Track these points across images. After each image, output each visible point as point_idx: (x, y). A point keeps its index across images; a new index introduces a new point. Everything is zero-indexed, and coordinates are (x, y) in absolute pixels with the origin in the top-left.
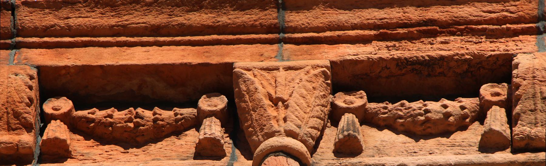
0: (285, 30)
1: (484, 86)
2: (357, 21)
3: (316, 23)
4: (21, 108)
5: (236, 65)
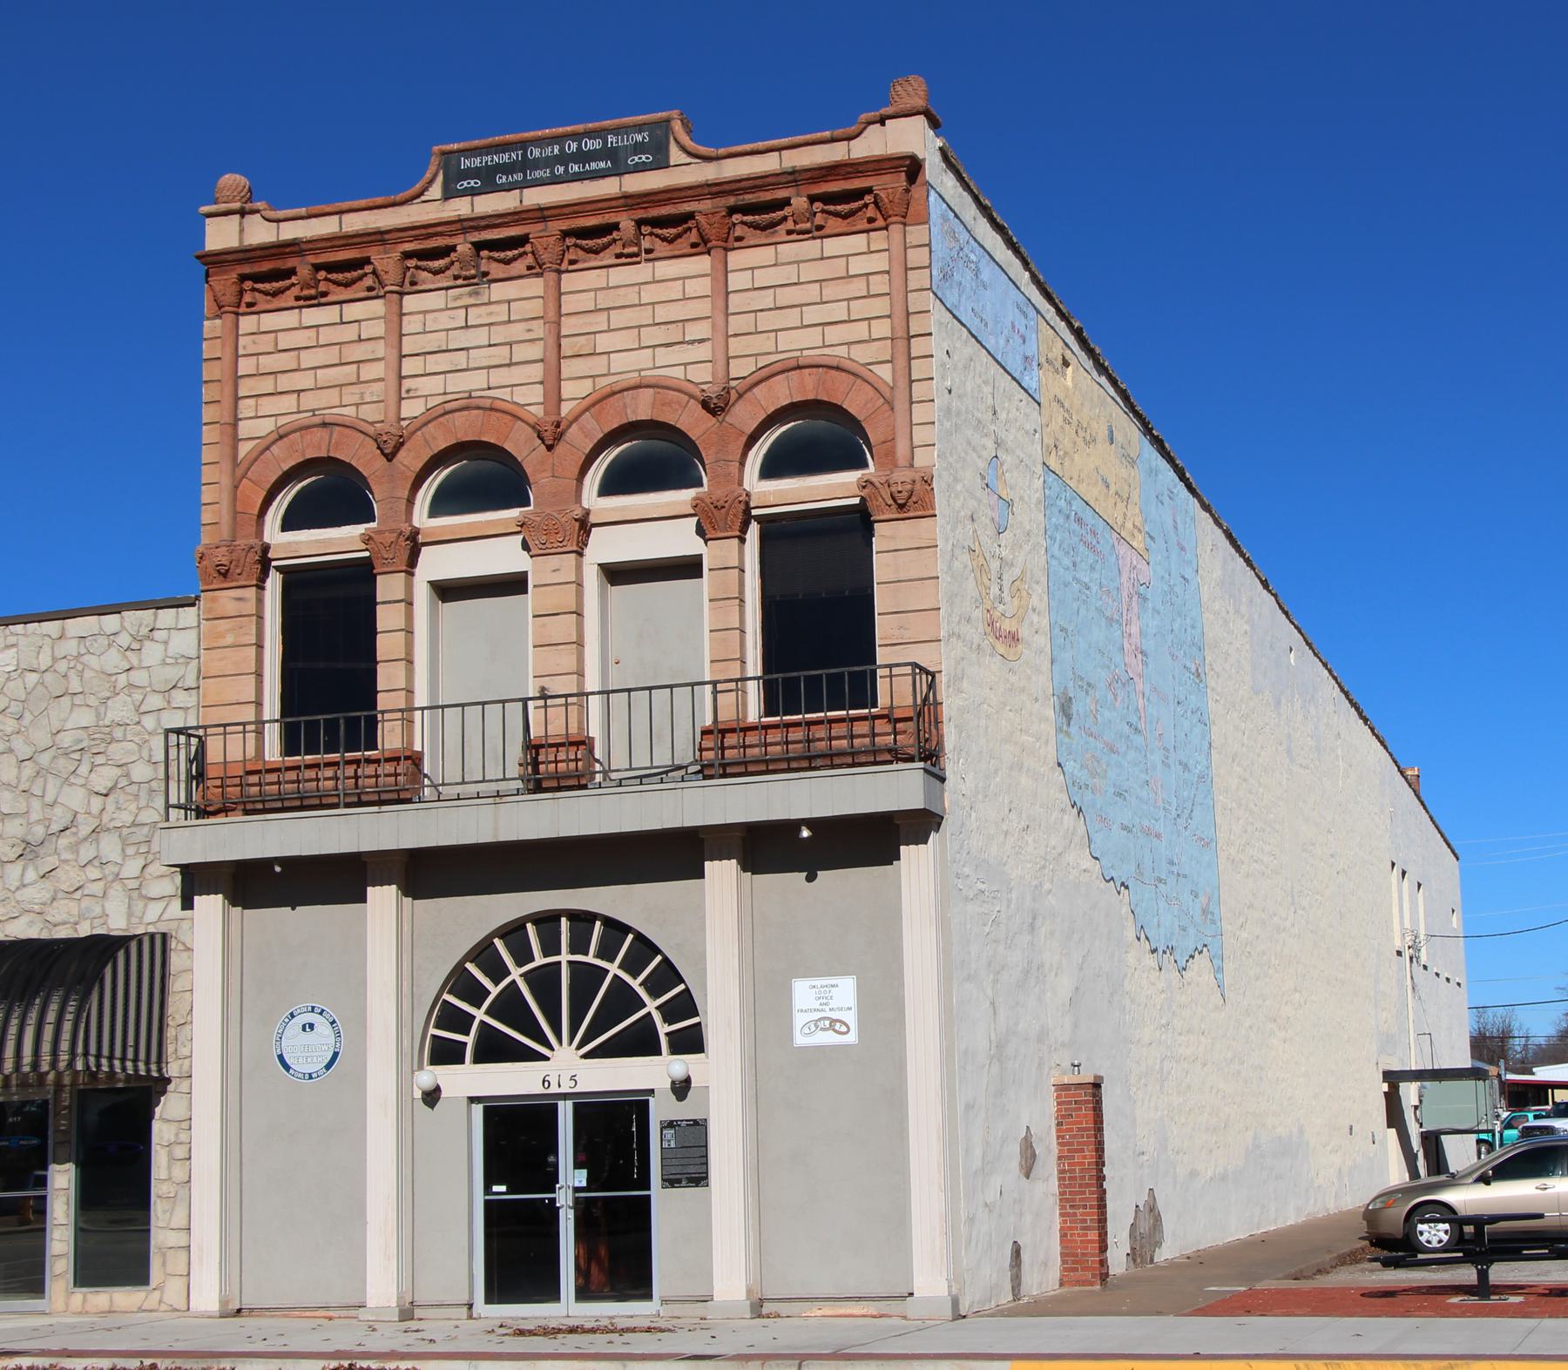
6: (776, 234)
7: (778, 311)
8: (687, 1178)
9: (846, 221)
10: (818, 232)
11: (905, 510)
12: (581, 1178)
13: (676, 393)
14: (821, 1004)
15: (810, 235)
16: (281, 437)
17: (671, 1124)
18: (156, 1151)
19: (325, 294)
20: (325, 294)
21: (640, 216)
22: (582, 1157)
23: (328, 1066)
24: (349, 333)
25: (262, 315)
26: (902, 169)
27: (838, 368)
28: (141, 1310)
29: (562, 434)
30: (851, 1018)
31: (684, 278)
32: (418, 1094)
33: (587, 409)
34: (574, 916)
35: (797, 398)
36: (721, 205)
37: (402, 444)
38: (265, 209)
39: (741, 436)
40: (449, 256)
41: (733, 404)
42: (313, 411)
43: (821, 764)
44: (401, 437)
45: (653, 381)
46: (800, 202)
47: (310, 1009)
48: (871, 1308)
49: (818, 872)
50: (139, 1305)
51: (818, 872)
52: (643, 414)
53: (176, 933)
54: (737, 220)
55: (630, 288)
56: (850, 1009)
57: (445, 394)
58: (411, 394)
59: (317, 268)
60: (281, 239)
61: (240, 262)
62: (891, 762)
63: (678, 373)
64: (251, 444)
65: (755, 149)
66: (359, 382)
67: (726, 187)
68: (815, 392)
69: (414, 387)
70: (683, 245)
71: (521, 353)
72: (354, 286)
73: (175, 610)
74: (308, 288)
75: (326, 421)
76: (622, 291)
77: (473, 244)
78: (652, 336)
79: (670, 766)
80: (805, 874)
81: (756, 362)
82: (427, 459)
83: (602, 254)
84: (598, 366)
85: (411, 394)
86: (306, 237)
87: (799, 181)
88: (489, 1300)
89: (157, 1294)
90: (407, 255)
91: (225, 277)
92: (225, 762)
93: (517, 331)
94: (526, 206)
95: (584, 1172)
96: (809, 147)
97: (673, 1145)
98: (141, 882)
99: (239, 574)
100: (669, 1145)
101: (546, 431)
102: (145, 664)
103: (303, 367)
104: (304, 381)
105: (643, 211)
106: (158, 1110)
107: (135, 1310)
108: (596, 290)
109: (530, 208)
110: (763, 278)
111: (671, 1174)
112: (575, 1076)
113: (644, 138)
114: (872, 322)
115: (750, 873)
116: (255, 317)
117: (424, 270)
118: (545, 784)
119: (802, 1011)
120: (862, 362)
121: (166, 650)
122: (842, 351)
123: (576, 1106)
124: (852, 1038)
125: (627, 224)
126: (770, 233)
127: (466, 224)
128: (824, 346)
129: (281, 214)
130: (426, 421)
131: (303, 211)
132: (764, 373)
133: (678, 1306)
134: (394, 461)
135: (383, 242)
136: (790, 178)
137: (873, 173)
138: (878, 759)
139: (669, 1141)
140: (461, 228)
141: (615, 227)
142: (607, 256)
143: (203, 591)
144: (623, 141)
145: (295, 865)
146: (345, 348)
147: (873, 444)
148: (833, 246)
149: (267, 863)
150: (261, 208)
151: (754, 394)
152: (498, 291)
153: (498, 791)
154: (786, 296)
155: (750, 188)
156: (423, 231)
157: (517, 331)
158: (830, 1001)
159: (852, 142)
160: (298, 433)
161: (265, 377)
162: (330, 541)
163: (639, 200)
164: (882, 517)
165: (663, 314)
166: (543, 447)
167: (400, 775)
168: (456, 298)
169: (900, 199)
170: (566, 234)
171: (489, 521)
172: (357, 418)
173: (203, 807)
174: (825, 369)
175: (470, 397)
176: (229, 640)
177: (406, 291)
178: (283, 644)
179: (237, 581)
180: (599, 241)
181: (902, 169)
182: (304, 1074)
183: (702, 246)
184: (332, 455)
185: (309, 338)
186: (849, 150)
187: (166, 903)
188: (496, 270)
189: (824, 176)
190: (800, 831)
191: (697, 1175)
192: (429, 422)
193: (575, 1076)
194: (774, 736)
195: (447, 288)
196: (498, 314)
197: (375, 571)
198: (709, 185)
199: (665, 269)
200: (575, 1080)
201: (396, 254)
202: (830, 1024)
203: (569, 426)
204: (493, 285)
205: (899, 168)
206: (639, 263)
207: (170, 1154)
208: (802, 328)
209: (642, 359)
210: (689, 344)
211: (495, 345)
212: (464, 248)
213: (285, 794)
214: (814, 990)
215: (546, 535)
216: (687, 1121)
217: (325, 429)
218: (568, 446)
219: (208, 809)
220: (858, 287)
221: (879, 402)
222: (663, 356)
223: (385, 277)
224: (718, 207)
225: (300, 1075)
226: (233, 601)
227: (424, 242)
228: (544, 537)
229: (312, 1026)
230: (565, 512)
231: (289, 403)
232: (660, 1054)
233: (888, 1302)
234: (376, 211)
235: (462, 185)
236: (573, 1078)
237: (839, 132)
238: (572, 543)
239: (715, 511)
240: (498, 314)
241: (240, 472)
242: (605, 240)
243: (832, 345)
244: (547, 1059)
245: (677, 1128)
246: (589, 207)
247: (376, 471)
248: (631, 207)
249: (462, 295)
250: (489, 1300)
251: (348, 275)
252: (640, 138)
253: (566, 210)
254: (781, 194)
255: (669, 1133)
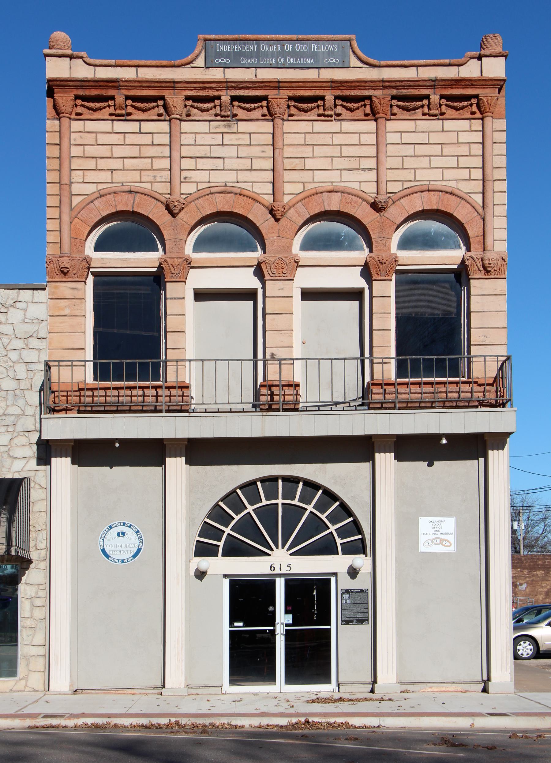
0: (175, 87)
1: (216, 101)
2: (190, 86)
3: (182, 86)
4: (122, 106)
5: (165, 96)
6: (416, 114)
7: (416, 158)
8: (356, 620)
9: (458, 112)
10: (125, 117)
11: (489, 274)
12: (289, 619)
13: (354, 197)
14: (435, 531)
15: (437, 117)
16: (101, 196)
17: (347, 591)
18: (22, 602)
19: (129, 114)
20: (129, 114)
21: (338, 94)
22: (290, 608)
23: (134, 556)
24: (147, 139)
25: (86, 122)
26: (497, 86)
27: (451, 193)
28: (12, 691)
29: (285, 213)
30: (452, 539)
31: (360, 133)
32: (192, 572)
33: (300, 201)
34: (287, 479)
35: (426, 208)
36: (388, 94)
37: (183, 208)
38: (86, 57)
39: (394, 225)
40: (214, 102)
41: (389, 207)
42: (122, 183)
43: (438, 405)
44: (184, 204)
45: (341, 189)
46: (435, 98)
47: (122, 524)
48: (460, 687)
49: (435, 462)
50: (11, 688)
51: (435, 462)
52: (334, 207)
53: (34, 478)
54: (128, 103)
55: (327, 135)
56: (451, 534)
57: (209, 182)
58: (187, 180)
59: (127, 98)
60: (72, 76)
61: (77, 87)
62: (477, 407)
63: (356, 186)
64: (80, 198)
65: (403, 64)
66: (152, 169)
67: (394, 84)
68: (437, 205)
69: (189, 176)
70: (359, 114)
71: (257, 164)
72: (149, 112)
73: (32, 291)
74: (120, 109)
75: (132, 190)
76: (322, 136)
77: (231, 96)
78: (339, 163)
79: (330, 402)
80: (428, 462)
81: (403, 185)
82: (198, 219)
83: (309, 113)
84: (306, 176)
85: (187, 180)
86: (125, 78)
87: (437, 86)
88: (233, 682)
89: (23, 682)
90: (187, 98)
91: (66, 95)
92: (485, 378)
93: (255, 151)
94: (420, 78)
95: (290, 616)
96: (435, 67)
97: (348, 602)
98: (9, 448)
99: (74, 274)
100: (346, 602)
101: (279, 210)
102: (10, 321)
103: (114, 156)
104: (116, 164)
105: (340, 91)
106: (24, 578)
107: (8, 691)
108: (305, 133)
109: (273, 80)
110: (407, 138)
111: (347, 618)
112: (290, 565)
113: (334, 48)
114: (472, 170)
115: (77, 466)
116: (82, 122)
117: (195, 108)
118: (398, 405)
119: (424, 534)
120: (465, 192)
121: (25, 315)
122: (453, 184)
123: (286, 581)
124: (452, 549)
125: (329, 97)
126: (412, 113)
127: (229, 84)
128: (443, 180)
129: (98, 62)
130: (199, 197)
131: (113, 62)
132: (408, 191)
133: (350, 686)
134: (177, 217)
135: (174, 88)
136: (433, 83)
137: (480, 87)
138: (470, 405)
139: (346, 600)
140: (226, 86)
141: (323, 98)
142: (313, 114)
143: (48, 282)
144: (321, 48)
145: (126, 443)
146: (143, 148)
147: (470, 237)
148: (449, 125)
149: (112, 441)
150: (84, 56)
151: (401, 203)
152: (243, 126)
153: (243, 409)
154: (421, 150)
155: (407, 86)
156: (201, 85)
157: (255, 151)
158: (440, 529)
159: (460, 68)
160: (112, 195)
161: (88, 159)
162: (130, 260)
163: (339, 85)
164: (475, 277)
165: (346, 151)
166: (273, 219)
167: (282, 395)
168: (216, 128)
169: (494, 103)
170: (290, 98)
171: (235, 258)
172: (151, 190)
173: (53, 407)
174: (443, 193)
175: (226, 186)
176: (67, 311)
177: (184, 119)
178: (94, 317)
179: (72, 277)
180: (310, 105)
181: (497, 86)
182: (119, 560)
183: (374, 115)
184: (135, 210)
185: (119, 139)
186: (458, 72)
187: (26, 461)
188: (242, 114)
189: (452, 85)
190: (115, 444)
191: (362, 618)
192: (200, 197)
193: (290, 565)
194: (402, 389)
195: (210, 121)
196: (243, 139)
197: (166, 280)
198: (384, 81)
199: (347, 126)
200: (290, 567)
201: (182, 97)
202: (440, 542)
203: (289, 209)
204: (239, 123)
205: (496, 85)
206: (332, 121)
207: (33, 605)
208: (430, 169)
209: (335, 176)
210: (362, 170)
211: (241, 158)
212: (226, 99)
213: (87, 403)
214: (432, 523)
215: (276, 269)
216: (356, 590)
217: (130, 195)
218: (289, 221)
219: (56, 408)
220: (464, 150)
221: (474, 214)
222: (347, 176)
223: (173, 109)
224: (386, 95)
225: (116, 561)
226: (69, 289)
227: (199, 91)
228: (275, 270)
229: (123, 534)
230: (289, 257)
231: (105, 176)
232: (338, 554)
233: (470, 685)
234: (160, 69)
235: (218, 61)
236: (289, 566)
237: (454, 61)
238: (291, 275)
239: (380, 265)
240: (243, 139)
241: (74, 214)
242: (256, 105)
243: (447, 180)
244: (269, 555)
245: (351, 593)
246: (308, 85)
247: (165, 222)
248: (333, 88)
249: (220, 126)
250: (233, 682)
251: (147, 105)
252: (332, 48)
253: (293, 85)
254: (425, 92)
255: (346, 596)
